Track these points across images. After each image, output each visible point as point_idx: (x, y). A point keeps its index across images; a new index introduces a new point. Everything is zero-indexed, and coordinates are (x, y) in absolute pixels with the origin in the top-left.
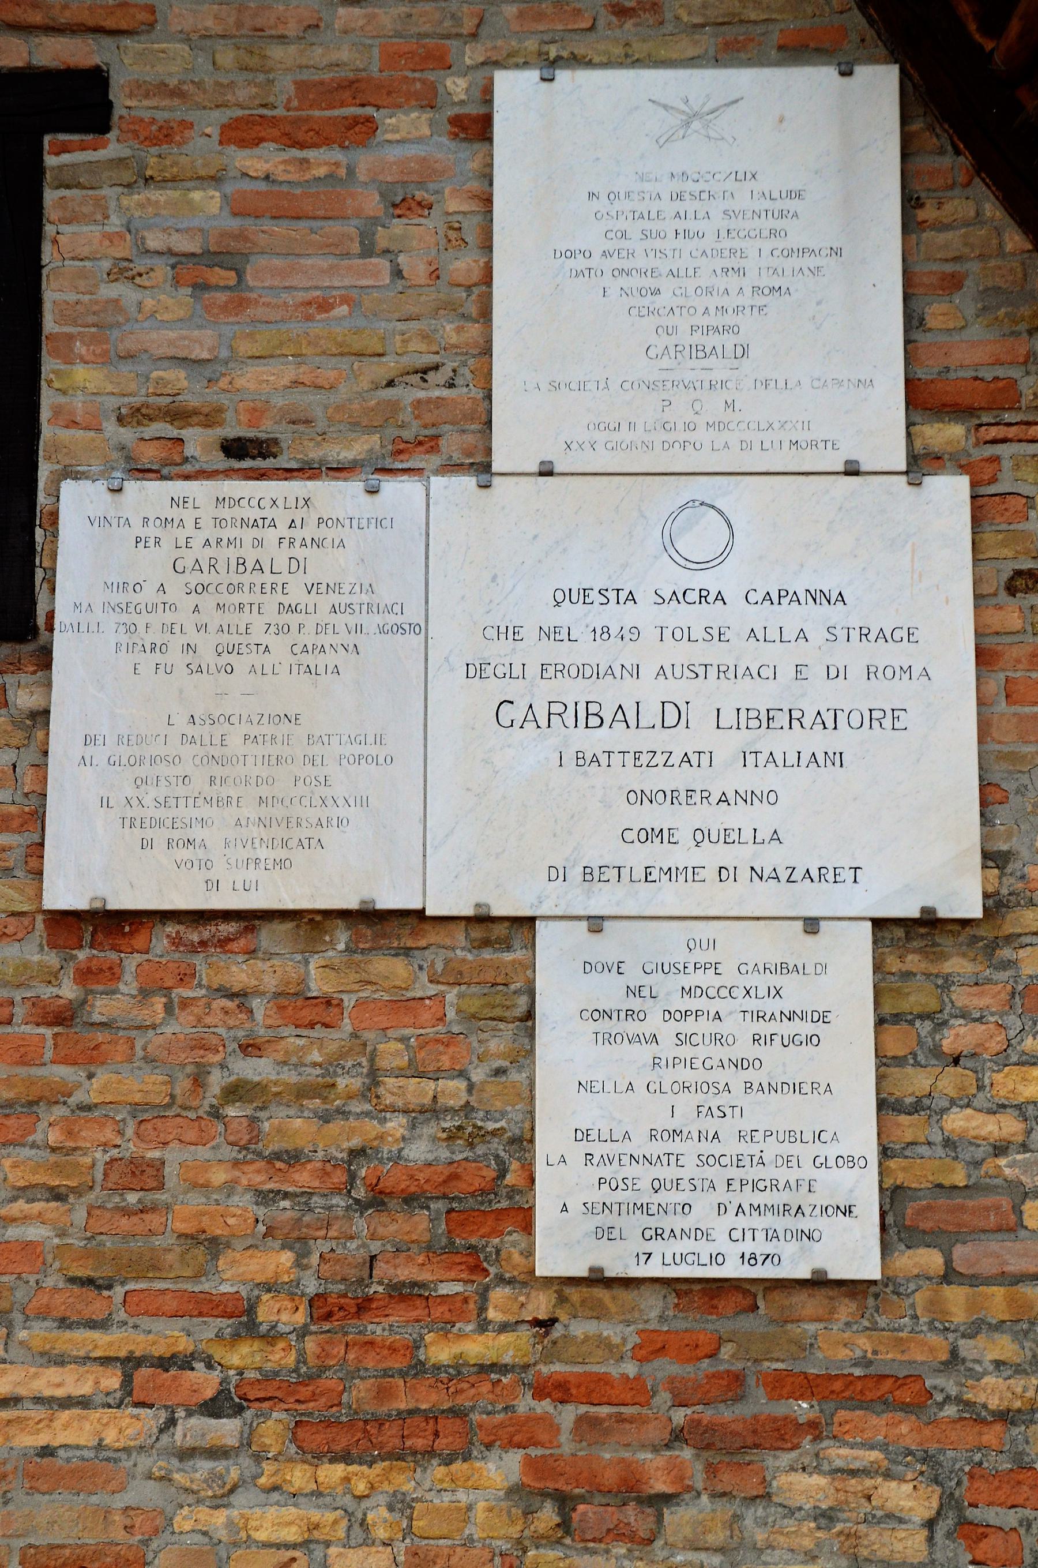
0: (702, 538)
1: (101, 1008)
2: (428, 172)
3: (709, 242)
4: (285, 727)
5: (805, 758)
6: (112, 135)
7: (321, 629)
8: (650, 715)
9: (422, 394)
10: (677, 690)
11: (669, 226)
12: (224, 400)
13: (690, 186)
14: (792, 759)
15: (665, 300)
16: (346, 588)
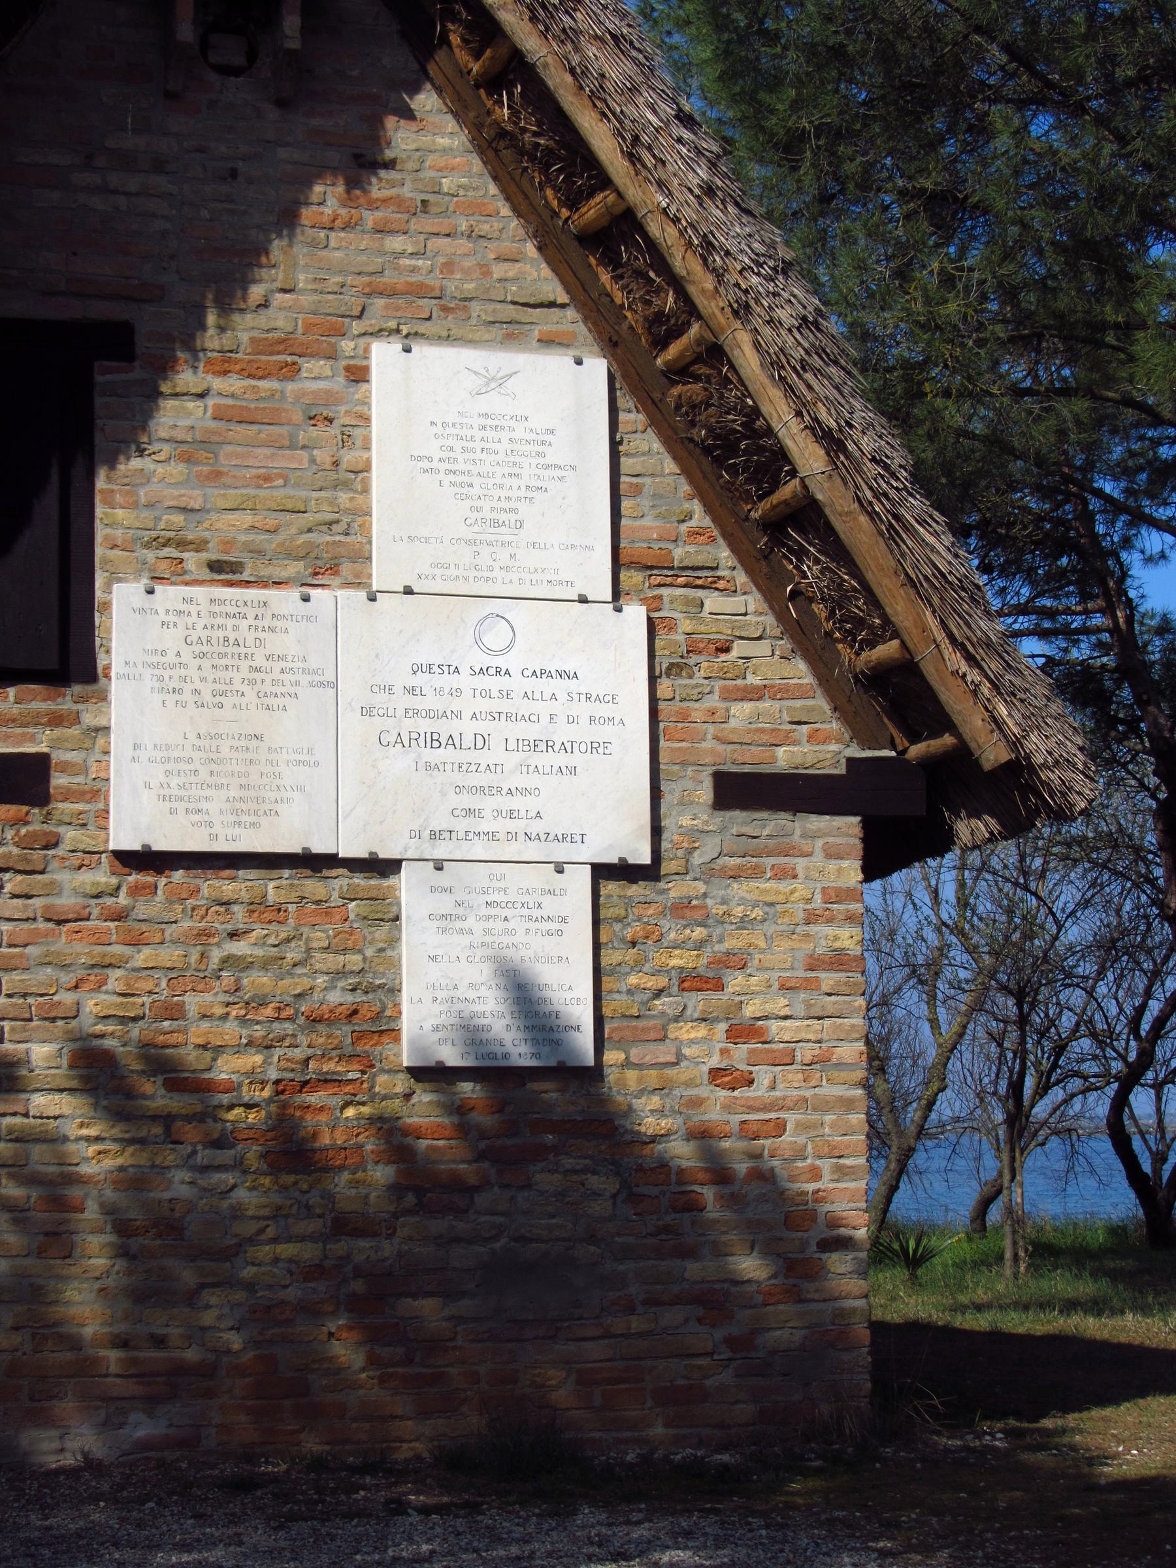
0: (497, 636)
1: (143, 909)
2: (332, 398)
3: (501, 457)
4: (254, 742)
5: (555, 769)
6: (137, 364)
7: (275, 682)
8: (468, 741)
9: (328, 538)
10: (483, 727)
11: (479, 445)
12: (207, 534)
13: (489, 422)
14: (547, 770)
15: (476, 491)
16: (290, 658)
